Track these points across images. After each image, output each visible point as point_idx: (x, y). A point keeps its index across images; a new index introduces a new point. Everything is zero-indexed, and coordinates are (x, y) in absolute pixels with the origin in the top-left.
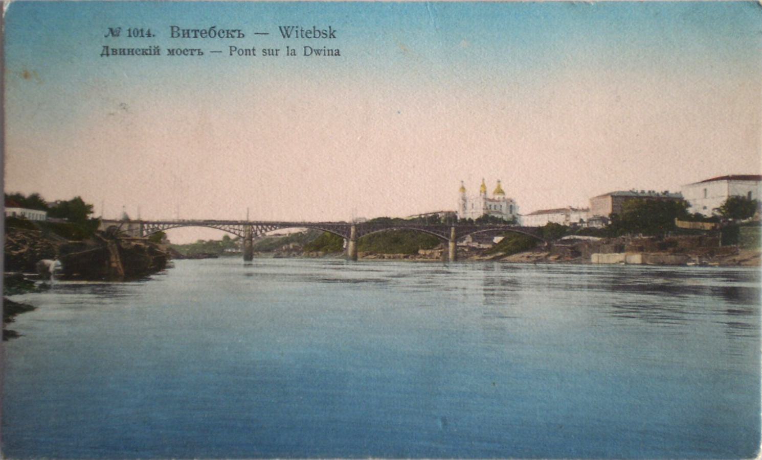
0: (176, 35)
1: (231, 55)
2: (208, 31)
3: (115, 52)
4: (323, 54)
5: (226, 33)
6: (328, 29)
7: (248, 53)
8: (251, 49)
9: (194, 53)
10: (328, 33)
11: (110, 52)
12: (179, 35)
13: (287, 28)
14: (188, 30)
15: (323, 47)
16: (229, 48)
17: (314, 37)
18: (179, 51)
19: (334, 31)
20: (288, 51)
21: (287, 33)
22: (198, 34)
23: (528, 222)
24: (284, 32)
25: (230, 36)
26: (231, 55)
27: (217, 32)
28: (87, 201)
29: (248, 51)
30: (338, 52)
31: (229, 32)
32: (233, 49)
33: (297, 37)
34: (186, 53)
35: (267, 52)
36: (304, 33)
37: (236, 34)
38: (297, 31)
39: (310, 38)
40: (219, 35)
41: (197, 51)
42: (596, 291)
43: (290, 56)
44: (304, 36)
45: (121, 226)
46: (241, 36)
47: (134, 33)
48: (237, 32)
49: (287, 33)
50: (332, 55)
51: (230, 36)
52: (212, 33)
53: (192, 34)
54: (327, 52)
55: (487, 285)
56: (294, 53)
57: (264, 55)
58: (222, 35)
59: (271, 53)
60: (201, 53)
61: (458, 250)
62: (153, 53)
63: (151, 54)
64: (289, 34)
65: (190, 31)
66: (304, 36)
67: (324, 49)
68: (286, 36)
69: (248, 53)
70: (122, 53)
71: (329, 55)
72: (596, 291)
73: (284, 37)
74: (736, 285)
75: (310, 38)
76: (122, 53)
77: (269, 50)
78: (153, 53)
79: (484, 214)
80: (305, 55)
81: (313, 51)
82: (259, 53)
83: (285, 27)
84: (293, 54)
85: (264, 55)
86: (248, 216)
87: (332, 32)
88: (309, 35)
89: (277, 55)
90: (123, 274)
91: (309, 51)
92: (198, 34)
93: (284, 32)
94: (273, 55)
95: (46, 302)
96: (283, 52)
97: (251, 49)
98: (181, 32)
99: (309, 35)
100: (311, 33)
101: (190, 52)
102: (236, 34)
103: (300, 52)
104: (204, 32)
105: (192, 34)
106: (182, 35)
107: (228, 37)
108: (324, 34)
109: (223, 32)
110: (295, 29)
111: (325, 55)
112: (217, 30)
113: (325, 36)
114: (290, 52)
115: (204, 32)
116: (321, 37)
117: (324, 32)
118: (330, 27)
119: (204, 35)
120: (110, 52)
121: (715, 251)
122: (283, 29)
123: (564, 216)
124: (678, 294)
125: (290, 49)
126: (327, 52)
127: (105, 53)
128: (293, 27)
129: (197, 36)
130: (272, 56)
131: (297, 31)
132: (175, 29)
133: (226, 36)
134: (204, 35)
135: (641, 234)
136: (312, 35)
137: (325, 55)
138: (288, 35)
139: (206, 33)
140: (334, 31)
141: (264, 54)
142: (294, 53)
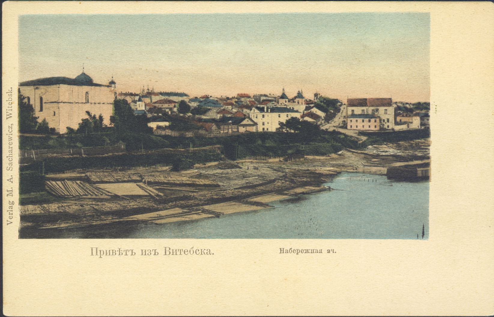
0: (168, 253)
12: (170, 252)
22: (182, 253)
25: (203, 253)
37: (153, 253)
40: (196, 253)
42: (54, 192)
45: (228, 131)
51: (203, 253)
52: (192, 252)
53: (178, 253)
55: (219, 216)
58: (198, 252)
72: (54, 192)
73: (12, 140)
79: (169, 125)
84: (208, 253)
90: (212, 146)
92: (182, 253)
95: (313, 197)
98: (171, 251)
103: (161, 252)
104: (186, 251)
105: (178, 253)
106: (172, 253)
110: (8, 111)
115: (186, 251)
118: (7, 93)
123: (240, 131)
132: (168, 249)
133: (200, 253)
134: (186, 253)
135: (336, 131)
140: (9, 90)
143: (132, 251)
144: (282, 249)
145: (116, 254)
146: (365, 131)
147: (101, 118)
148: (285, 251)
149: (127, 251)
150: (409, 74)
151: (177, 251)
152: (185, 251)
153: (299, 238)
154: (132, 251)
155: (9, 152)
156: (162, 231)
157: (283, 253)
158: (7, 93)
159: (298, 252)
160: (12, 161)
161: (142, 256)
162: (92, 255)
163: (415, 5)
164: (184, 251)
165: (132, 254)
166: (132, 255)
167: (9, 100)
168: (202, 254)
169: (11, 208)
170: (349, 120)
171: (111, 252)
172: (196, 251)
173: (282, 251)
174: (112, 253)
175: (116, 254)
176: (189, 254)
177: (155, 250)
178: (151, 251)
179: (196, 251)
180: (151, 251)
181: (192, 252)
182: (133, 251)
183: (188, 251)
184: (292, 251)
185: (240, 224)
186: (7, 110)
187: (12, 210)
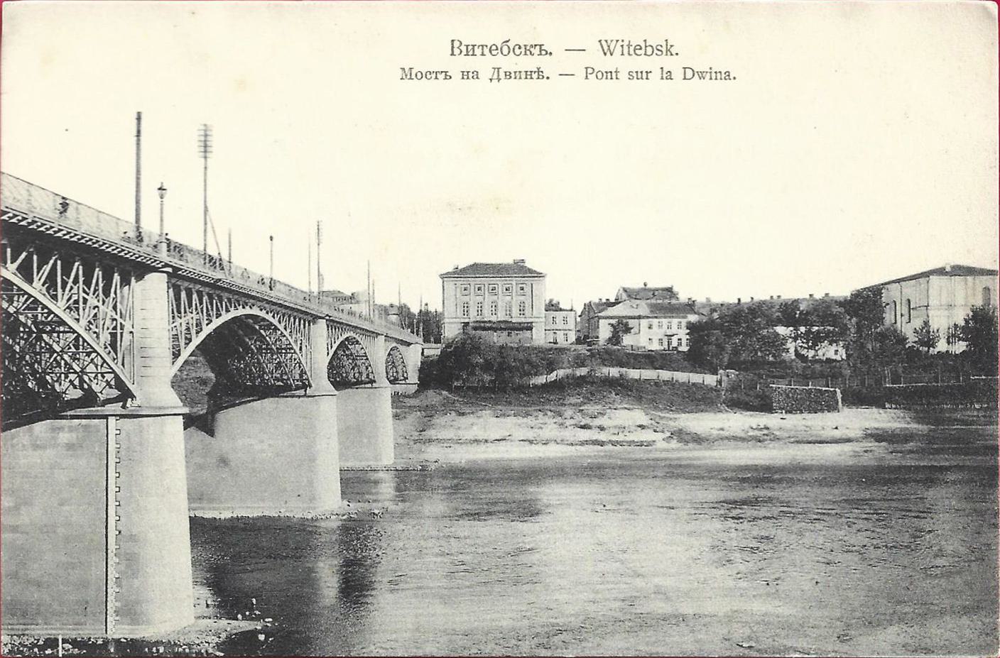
0: (457, 51)
1: (587, 78)
3: (508, 75)
4: (709, 78)
5: (523, 50)
6: (664, 44)
7: (609, 77)
8: (613, 71)
9: (439, 76)
10: (664, 49)
11: (502, 75)
13: (609, 42)
14: (474, 46)
15: (708, 68)
17: (645, 54)
19: (672, 46)
20: (662, 74)
21: (609, 49)
23: (217, 416)
24: (606, 48)
25: (528, 52)
26: (587, 78)
28: (587, 302)
29: (609, 74)
30: (670, 75)
31: (528, 48)
32: (590, 71)
33: (622, 54)
35: (635, 75)
36: (632, 49)
37: (536, 51)
38: (622, 46)
39: (640, 55)
43: (724, 80)
44: (632, 52)
48: (538, 47)
49: (609, 49)
50: (721, 79)
51: (528, 52)
52: (505, 50)
54: (714, 75)
56: (669, 76)
57: (629, 79)
58: (517, 51)
59: (639, 77)
60: (448, 77)
64: (612, 51)
65: (476, 47)
66: (632, 52)
67: (709, 71)
68: (608, 54)
69: (609, 77)
71: (716, 79)
73: (605, 54)
75: (640, 55)
77: (637, 72)
80: (685, 79)
81: (696, 74)
82: (623, 75)
83: (606, 41)
85: (629, 79)
87: (669, 47)
88: (637, 52)
89: (647, 79)
91: (689, 74)
92: (486, 51)
93: (606, 48)
94: (642, 78)
96: (656, 74)
97: (613, 71)
98: (464, 48)
99: (637, 52)
100: (641, 49)
101: (434, 76)
102: (536, 51)
104: (494, 47)
105: (478, 51)
107: (526, 54)
108: (658, 50)
110: (620, 43)
111: (711, 79)
112: (511, 44)
113: (659, 53)
114: (665, 76)
115: (494, 47)
116: (654, 54)
117: (659, 48)
119: (494, 52)
120: (502, 75)
121: (571, 502)
122: (603, 43)
125: (665, 71)
126: (714, 75)
127: (495, 76)
128: (617, 41)
129: (485, 53)
130: (641, 80)
131: (622, 46)
132: (456, 44)
133: (523, 53)
134: (494, 52)
136: (642, 52)
137: (711, 79)
138: (610, 51)
139: (497, 49)
140: (672, 46)
141: (631, 77)
142: (477, 75)
143: (540, 48)
146: (44, 268)
150: (267, 338)
152: (491, 47)
155: (725, 73)
158: (645, 41)
160: (634, 55)
163: (701, 650)
164: (489, 47)
167: (646, 47)
168: (526, 54)
169: (669, 77)
170: (791, 340)
172: (514, 49)
179: (514, 49)
181: (505, 50)
185: (473, 499)
186: (623, 41)
187: (664, 77)
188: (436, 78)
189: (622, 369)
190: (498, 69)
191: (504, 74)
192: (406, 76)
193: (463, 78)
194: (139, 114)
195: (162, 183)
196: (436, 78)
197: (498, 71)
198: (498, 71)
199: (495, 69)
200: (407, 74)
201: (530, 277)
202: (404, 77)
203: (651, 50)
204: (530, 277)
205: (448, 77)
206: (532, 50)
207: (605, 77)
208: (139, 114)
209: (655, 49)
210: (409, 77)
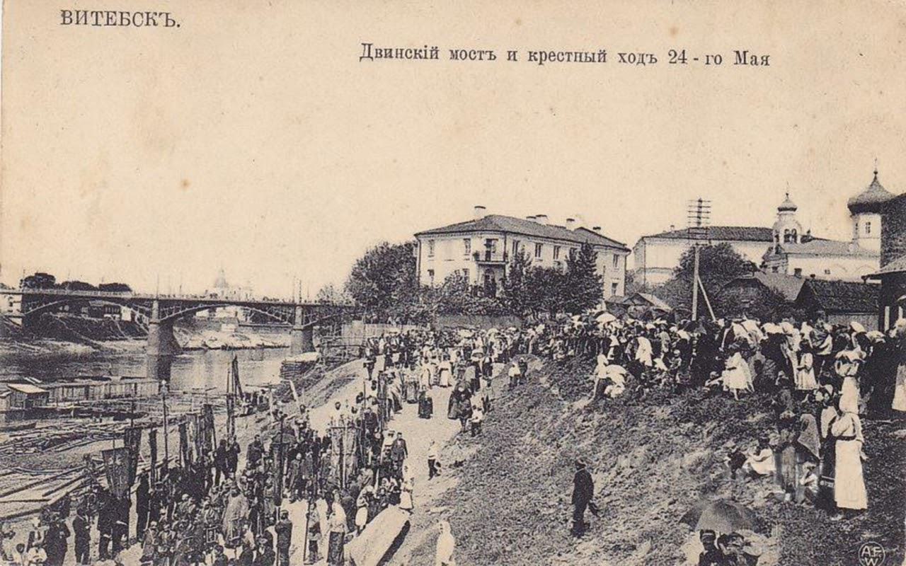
0: (68, 20)
2: (556, 55)
11: (373, 54)
12: (381, 56)
16: (528, 54)
18: (463, 54)
22: (572, 58)
25: (151, 22)
27: (468, 57)
34: (561, 58)
37: (647, 60)
41: (488, 54)
46: (654, 60)
47: (461, 55)
53: (91, 20)
60: (492, 57)
61: (561, 341)
62: (429, 56)
63: (426, 58)
70: (512, 58)
74: (697, 264)
76: (512, 58)
78: (429, 56)
84: (754, 62)
86: (18, 302)
96: (663, 58)
104: (552, 54)
105: (91, 20)
106: (75, 21)
109: (411, 52)
120: (373, 54)
124: (32, 376)
134: (552, 58)
139: (554, 56)
143: (167, 17)
144: (399, 56)
145: (752, 58)
147: (677, 267)
148: (751, 60)
149: (99, 14)
151: (89, 14)
153: (902, 195)
154: (167, 17)
156: (812, 557)
157: (386, 50)
159: (543, 58)
161: (510, 62)
162: (97, 24)
165: (64, 20)
166: (167, 25)
168: (148, 24)
171: (583, 56)
173: (371, 53)
174: (120, 20)
175: (762, 58)
176: (548, 54)
177: (167, 14)
178: (71, 14)
180: (71, 14)
182: (169, 16)
183: (554, 56)
184: (468, 54)
188: (481, 59)
189: (361, 495)
190: (370, 45)
191: (375, 51)
192: (740, 60)
193: (509, 59)
194: (484, 208)
195: (206, 564)
196: (481, 59)
197: (369, 48)
198: (369, 48)
199: (365, 45)
200: (371, 53)
201: (228, 384)
202: (738, 62)
203: (136, 23)
204: (228, 384)
205: (492, 57)
206: (155, 17)
207: (459, 53)
208: (484, 208)
209: (131, 20)
210: (743, 61)
